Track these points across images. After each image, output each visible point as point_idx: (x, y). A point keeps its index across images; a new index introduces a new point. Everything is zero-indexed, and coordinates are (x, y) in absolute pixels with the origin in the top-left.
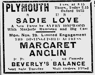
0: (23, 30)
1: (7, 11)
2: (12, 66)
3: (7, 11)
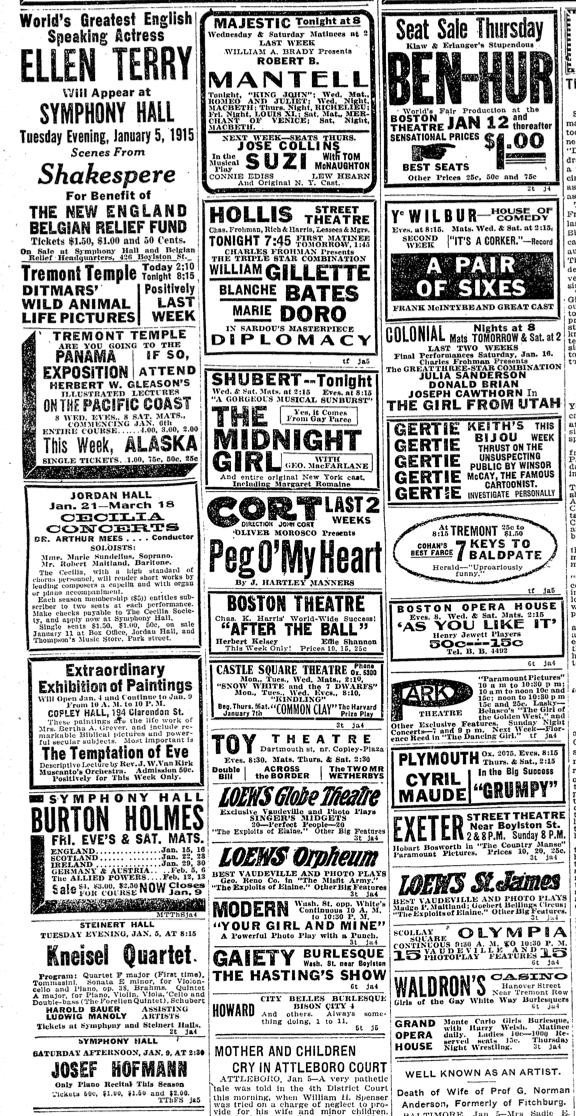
1: (212, 569)
2: (230, 609)
3: (212, 569)
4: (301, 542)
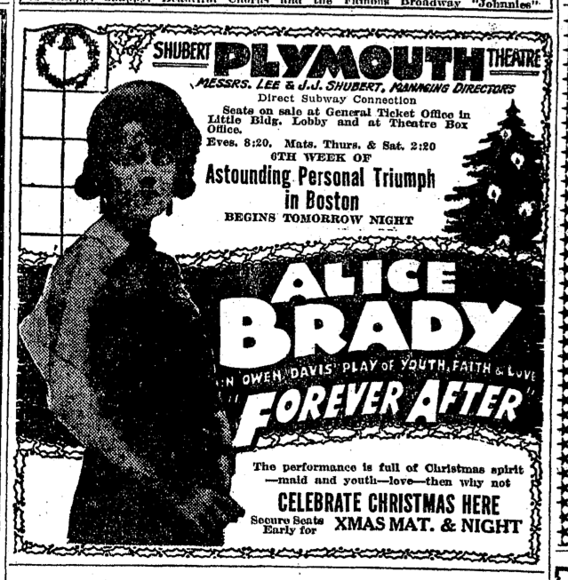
0: (295, 145)
4: (450, 61)
